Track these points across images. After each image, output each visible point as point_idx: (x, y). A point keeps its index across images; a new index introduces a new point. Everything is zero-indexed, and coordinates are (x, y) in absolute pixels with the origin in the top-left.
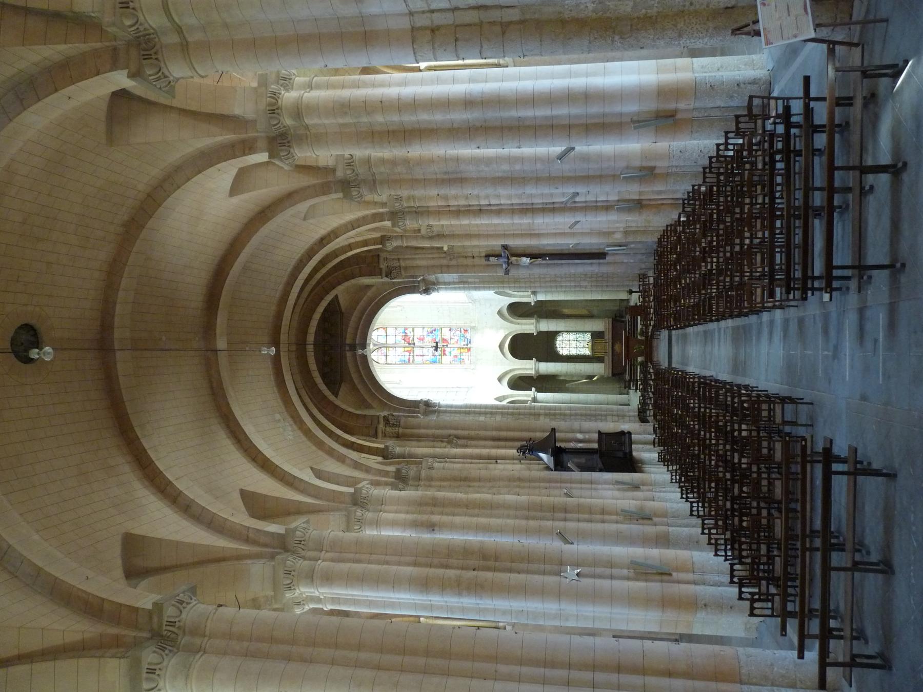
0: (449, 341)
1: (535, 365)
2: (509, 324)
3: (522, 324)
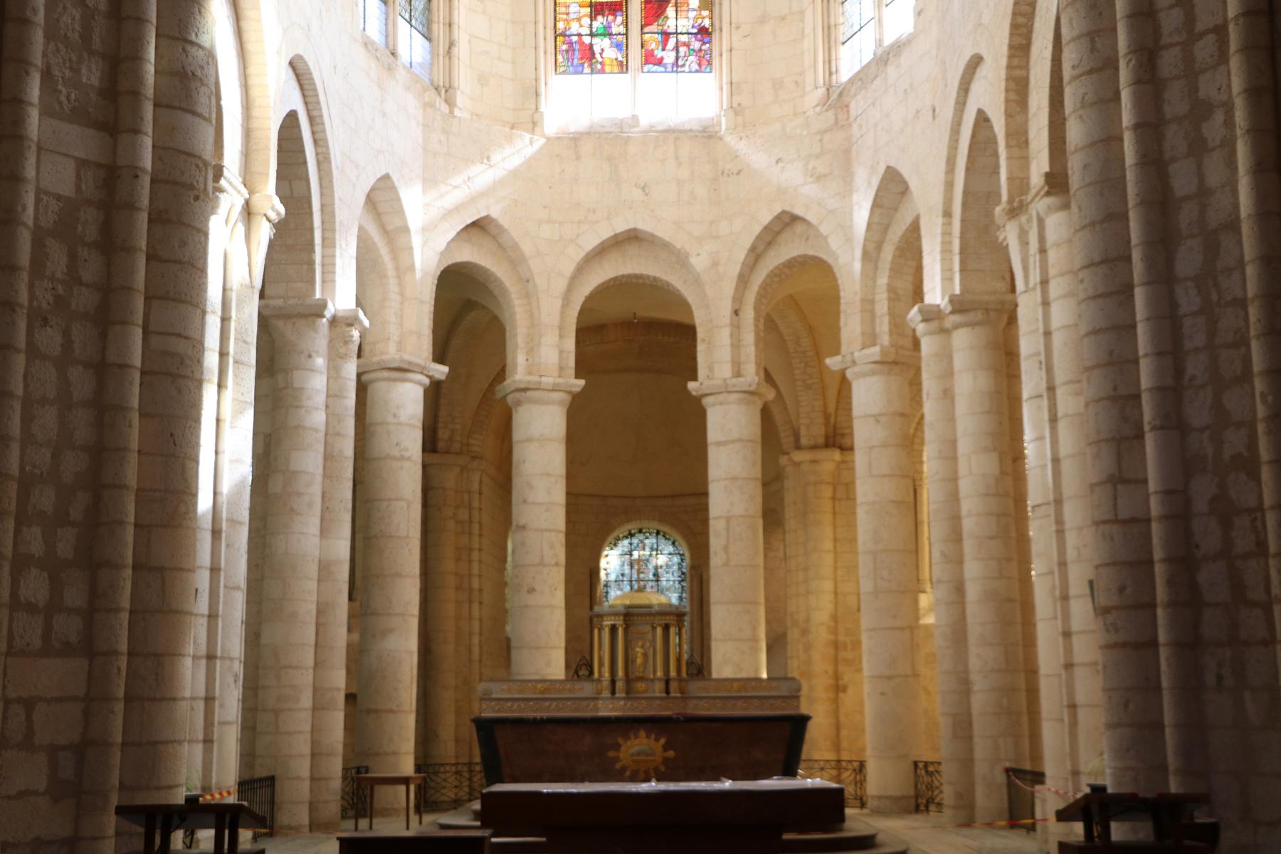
0: (654, 28)
1: (555, 389)
2: (735, 270)
3: (736, 327)
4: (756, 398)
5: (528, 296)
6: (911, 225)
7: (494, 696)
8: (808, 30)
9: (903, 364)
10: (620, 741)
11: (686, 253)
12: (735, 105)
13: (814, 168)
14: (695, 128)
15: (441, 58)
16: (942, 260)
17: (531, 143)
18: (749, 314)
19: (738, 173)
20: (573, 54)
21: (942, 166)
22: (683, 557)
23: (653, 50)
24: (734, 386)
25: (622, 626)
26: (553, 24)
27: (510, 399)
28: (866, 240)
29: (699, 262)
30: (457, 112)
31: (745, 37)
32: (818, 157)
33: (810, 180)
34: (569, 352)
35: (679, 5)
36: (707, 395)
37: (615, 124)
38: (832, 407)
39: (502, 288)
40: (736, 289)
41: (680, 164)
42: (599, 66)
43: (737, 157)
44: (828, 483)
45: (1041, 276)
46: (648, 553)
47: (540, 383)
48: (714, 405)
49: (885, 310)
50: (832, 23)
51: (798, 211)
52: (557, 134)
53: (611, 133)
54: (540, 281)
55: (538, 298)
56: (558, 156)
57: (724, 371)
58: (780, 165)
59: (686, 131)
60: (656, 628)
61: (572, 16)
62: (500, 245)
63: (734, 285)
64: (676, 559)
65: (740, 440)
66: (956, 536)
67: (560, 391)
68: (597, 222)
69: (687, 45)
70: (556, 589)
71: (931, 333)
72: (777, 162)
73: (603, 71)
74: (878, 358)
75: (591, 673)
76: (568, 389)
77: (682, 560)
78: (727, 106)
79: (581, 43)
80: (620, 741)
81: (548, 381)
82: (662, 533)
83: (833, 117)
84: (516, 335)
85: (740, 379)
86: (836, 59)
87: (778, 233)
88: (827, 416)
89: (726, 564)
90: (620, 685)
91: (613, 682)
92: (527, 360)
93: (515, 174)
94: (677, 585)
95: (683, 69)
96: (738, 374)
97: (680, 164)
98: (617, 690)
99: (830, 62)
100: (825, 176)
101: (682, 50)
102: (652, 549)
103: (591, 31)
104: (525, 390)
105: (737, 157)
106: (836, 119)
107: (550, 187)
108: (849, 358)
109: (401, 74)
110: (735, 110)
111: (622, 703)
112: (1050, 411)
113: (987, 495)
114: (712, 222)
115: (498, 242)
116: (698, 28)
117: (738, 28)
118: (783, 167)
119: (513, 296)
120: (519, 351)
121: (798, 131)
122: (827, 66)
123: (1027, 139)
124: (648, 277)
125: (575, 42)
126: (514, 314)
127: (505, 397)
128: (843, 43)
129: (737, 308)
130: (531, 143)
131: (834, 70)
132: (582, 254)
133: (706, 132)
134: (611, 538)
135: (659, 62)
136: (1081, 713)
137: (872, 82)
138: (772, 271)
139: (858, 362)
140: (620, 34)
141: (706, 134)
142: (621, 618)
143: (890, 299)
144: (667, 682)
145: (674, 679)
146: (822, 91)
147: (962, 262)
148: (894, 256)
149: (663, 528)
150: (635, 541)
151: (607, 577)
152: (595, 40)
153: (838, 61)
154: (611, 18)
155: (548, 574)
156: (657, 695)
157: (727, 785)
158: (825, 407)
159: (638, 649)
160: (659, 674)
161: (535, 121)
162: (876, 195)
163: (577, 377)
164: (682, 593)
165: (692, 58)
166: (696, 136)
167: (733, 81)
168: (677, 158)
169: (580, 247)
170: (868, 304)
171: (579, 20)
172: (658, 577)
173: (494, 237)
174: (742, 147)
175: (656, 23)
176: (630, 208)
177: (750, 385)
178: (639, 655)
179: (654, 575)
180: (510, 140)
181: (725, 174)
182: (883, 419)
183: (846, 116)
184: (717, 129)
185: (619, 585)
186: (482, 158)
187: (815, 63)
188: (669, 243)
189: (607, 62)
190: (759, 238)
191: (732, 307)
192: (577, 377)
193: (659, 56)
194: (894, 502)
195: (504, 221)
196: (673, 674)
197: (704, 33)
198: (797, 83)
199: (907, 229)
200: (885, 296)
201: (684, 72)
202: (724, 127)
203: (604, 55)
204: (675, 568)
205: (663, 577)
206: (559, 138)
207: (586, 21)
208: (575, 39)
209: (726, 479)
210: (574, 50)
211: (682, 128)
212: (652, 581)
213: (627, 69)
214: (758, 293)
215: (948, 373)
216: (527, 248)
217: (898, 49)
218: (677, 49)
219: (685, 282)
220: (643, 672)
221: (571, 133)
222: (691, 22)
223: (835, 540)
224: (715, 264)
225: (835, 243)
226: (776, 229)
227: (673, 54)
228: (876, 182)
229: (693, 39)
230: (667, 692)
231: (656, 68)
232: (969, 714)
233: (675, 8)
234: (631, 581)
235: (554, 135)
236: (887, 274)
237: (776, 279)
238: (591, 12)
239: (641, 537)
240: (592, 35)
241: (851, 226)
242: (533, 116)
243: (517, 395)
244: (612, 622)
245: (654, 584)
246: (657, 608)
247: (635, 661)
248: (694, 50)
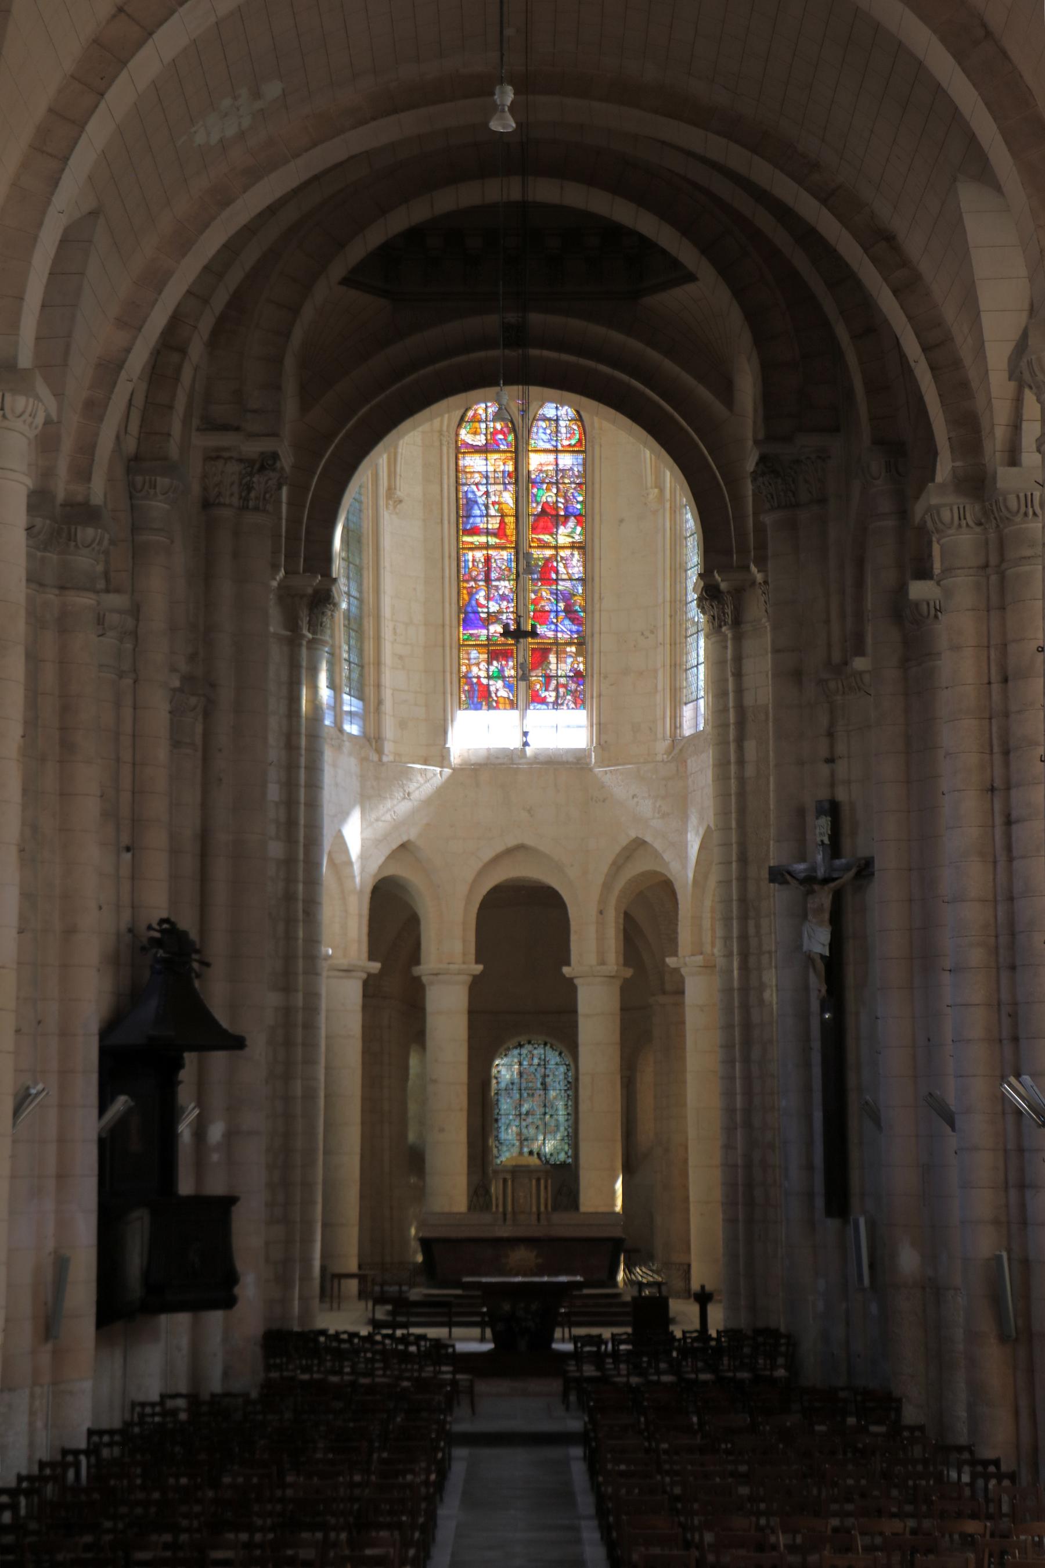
2: (601, 879)
8: (660, 687)
12: (602, 742)
13: (660, 806)
14: (571, 759)
15: (372, 715)
18: (611, 915)
19: (604, 801)
20: (474, 694)
22: (568, 1068)
23: (538, 691)
26: (457, 669)
30: (385, 759)
31: (611, 685)
33: (657, 815)
35: (559, 652)
42: (494, 704)
50: (678, 686)
53: (504, 764)
57: (591, 959)
61: (473, 661)
69: (565, 686)
72: (633, 797)
73: (497, 708)
77: (568, 1070)
79: (479, 683)
85: (604, 967)
86: (680, 717)
90: (509, 1216)
92: (438, 949)
95: (562, 707)
96: (602, 963)
99: (675, 717)
101: (562, 690)
103: (488, 674)
106: (678, 770)
109: (347, 744)
116: (574, 672)
117: (606, 677)
122: (673, 721)
125: (476, 683)
131: (678, 725)
132: (480, 865)
134: (502, 1050)
135: (543, 701)
140: (511, 677)
144: (539, 1214)
146: (668, 742)
150: (524, 1051)
151: (498, 1085)
152: (491, 682)
154: (504, 663)
157: (546, 1279)
159: (521, 1194)
163: (477, 962)
164: (567, 1101)
165: (569, 697)
166: (571, 768)
171: (478, 664)
175: (540, 669)
179: (542, 1084)
184: (588, 760)
185: (509, 1093)
189: (501, 700)
190: (619, 855)
192: (477, 962)
193: (543, 696)
196: (542, 1209)
197: (578, 676)
200: (709, 915)
201: (563, 709)
203: (499, 694)
204: (562, 1077)
207: (483, 665)
208: (475, 680)
210: (474, 691)
212: (540, 1090)
213: (517, 706)
218: (556, 690)
221: (472, 765)
222: (569, 667)
227: (554, 694)
229: (570, 682)
231: (539, 706)
233: (556, 655)
234: (520, 1090)
238: (488, 658)
239: (530, 1047)
240: (489, 677)
248: (571, 691)
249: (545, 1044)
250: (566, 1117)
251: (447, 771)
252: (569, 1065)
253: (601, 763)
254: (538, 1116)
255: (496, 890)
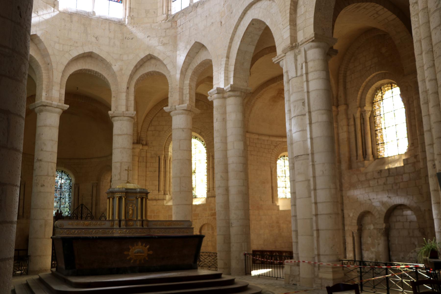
3: (128, 93)
4: (132, 120)
5: (48, 70)
6: (199, 64)
7: (64, 227)
9: (192, 112)
10: (130, 247)
11: (111, 64)
12: (131, 15)
13: (162, 41)
14: (116, 21)
16: (225, 73)
17: (54, 11)
18: (132, 90)
19: (132, 39)
21: (229, 40)
24: (126, 114)
25: (124, 197)
27: (36, 110)
28: (182, 67)
29: (115, 68)
32: (164, 37)
33: (160, 44)
34: (62, 94)
36: (115, 117)
37: (86, 13)
38: (139, 131)
39: (37, 65)
40: (129, 80)
41: (110, 32)
43: (132, 33)
44: (137, 156)
45: (306, 71)
46: (58, 178)
47: (52, 104)
48: (118, 120)
49: (188, 92)
51: (156, 55)
52: (63, 11)
53: (85, 15)
54: (54, 65)
55: (53, 71)
56: (63, 19)
57: (122, 109)
58: (149, 38)
59: (113, 21)
60: (138, 199)
62: (38, 48)
63: (128, 78)
64: (68, 181)
65: (127, 134)
66: (226, 171)
67: (59, 108)
68: (78, 47)
70: (52, 186)
71: (219, 98)
72: (148, 37)
74: (186, 108)
75: (106, 219)
76: (63, 108)
78: (128, 15)
80: (130, 247)
81: (55, 103)
82: (64, 172)
83: (171, 24)
84: (42, 84)
86: (170, 6)
87: (145, 62)
88: (138, 133)
89: (120, 179)
91: (120, 221)
92: (46, 95)
93: (47, 21)
94: (68, 190)
96: (127, 110)
97: (110, 32)
98: (122, 225)
99: (168, 7)
100: (166, 44)
102: (60, 177)
104: (45, 106)
105: (132, 33)
107: (60, 30)
108: (174, 107)
110: (131, 17)
111: (125, 230)
112: (309, 120)
113: (240, 156)
114: (121, 55)
115: (37, 46)
118: (150, 39)
119: (42, 69)
120: (43, 90)
121: (157, 27)
122: (167, 8)
123: (296, 24)
124: (94, 71)
126: (42, 76)
127: (34, 109)
128: (173, 2)
129: (128, 86)
130: (54, 11)
131: (169, 9)
132: (71, 58)
133: (120, 23)
136: (322, 233)
137: (189, 14)
138: (141, 75)
139: (177, 109)
141: (120, 24)
142: (124, 194)
143: (190, 89)
145: (123, 220)
146: (165, 16)
147: (234, 74)
148: (192, 74)
149: (64, 170)
153: (171, 7)
155: (50, 180)
156: (139, 227)
158: (137, 130)
159: (130, 208)
160: (139, 218)
161: (55, 4)
162: (189, 51)
163: (65, 103)
164: (70, 193)
166: (117, 23)
167: (131, 7)
168: (109, 30)
169: (70, 55)
170: (181, 89)
172: (61, 187)
173: (36, 44)
174: (134, 30)
176: (91, 44)
177: (132, 115)
178: (130, 210)
179: (60, 186)
180: (46, 8)
181: (127, 38)
182: (185, 130)
183: (175, 25)
184: (124, 22)
186: (35, 12)
187: (163, 6)
188: (104, 59)
190: (139, 62)
191: (127, 86)
192: (65, 103)
194: (187, 159)
195: (42, 38)
196: (123, 218)
198: (154, 12)
199: (198, 65)
200: (188, 87)
202: (126, 22)
204: (68, 184)
205: (63, 187)
206: (64, 13)
209: (121, 148)
211: (111, 19)
214: (136, 83)
215: (225, 113)
216: (50, 51)
217: (203, 3)
219: (108, 75)
220: (132, 217)
223: (138, 176)
224: (121, 70)
225: (169, 67)
226: (145, 60)
228: (189, 47)
230: (142, 226)
232: (229, 235)
235: (62, 11)
236: (189, 80)
237: (142, 79)
241: (176, 62)
242: (54, 2)
243: (42, 108)
244: (120, 196)
245: (60, 189)
246: (138, 190)
247: (129, 213)
249: (62, 172)
250: (69, 199)
251: (57, 13)
252: (71, 180)
253: (130, 23)
254: (58, 198)
255: (71, 76)
